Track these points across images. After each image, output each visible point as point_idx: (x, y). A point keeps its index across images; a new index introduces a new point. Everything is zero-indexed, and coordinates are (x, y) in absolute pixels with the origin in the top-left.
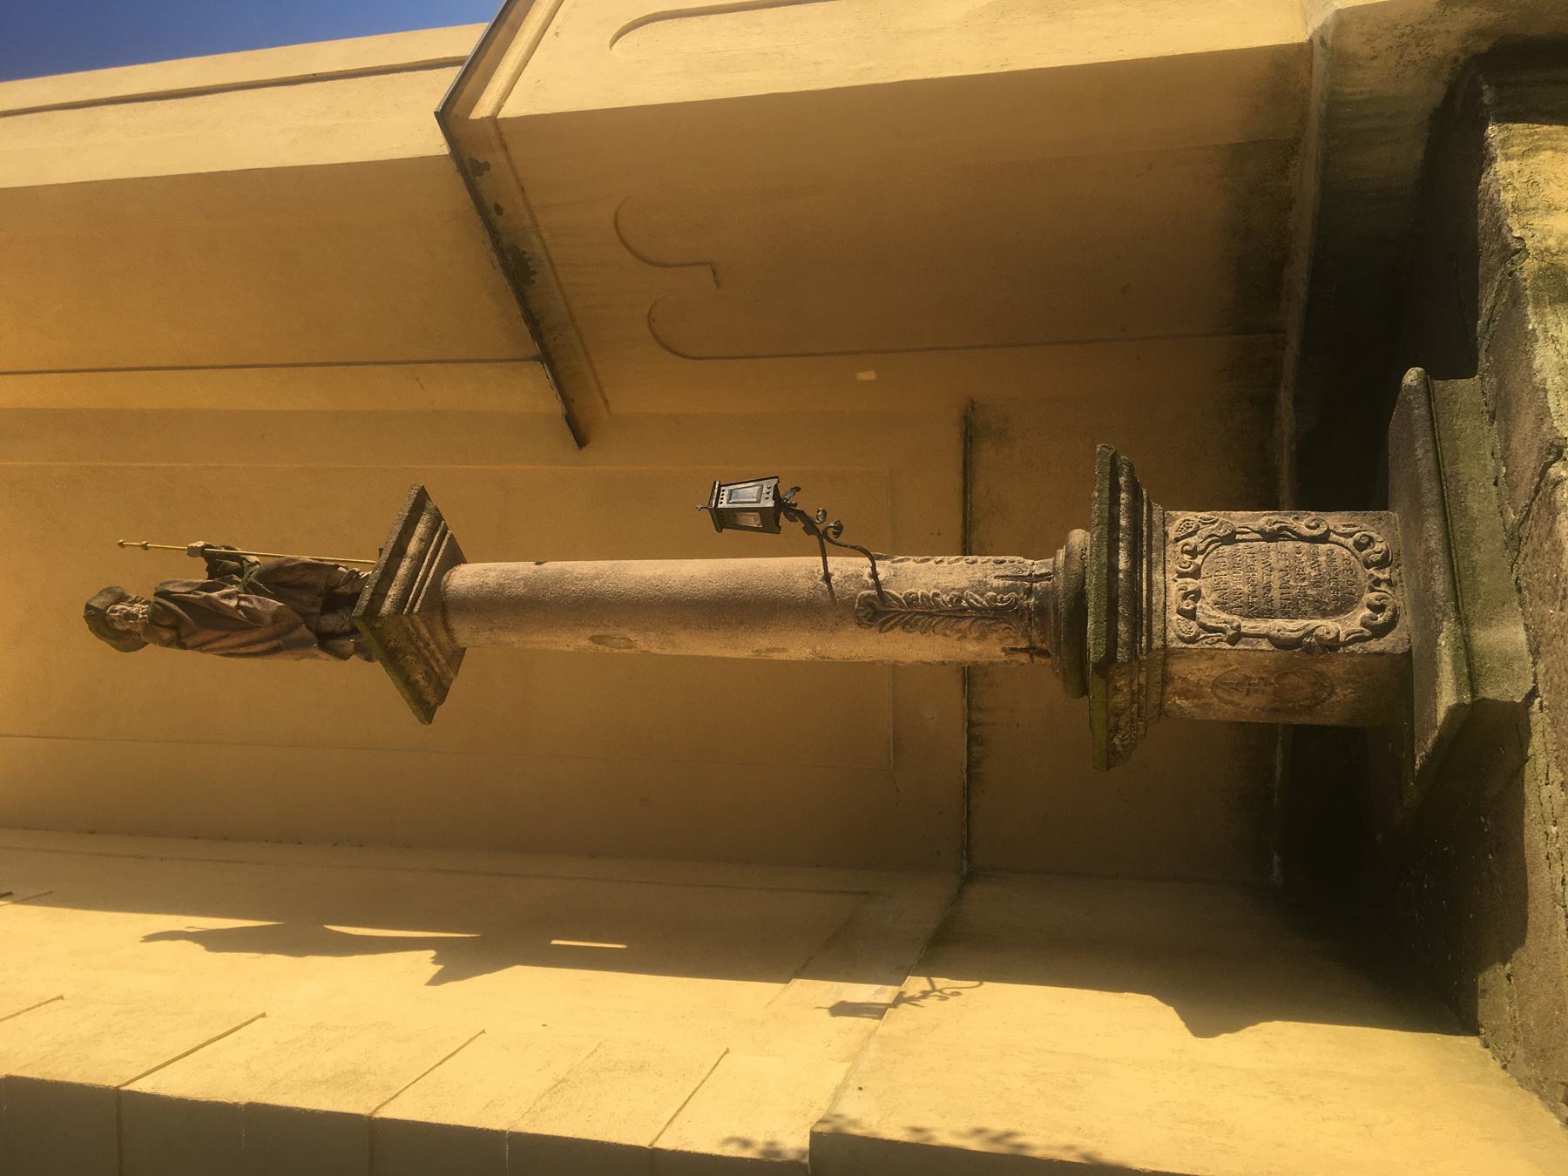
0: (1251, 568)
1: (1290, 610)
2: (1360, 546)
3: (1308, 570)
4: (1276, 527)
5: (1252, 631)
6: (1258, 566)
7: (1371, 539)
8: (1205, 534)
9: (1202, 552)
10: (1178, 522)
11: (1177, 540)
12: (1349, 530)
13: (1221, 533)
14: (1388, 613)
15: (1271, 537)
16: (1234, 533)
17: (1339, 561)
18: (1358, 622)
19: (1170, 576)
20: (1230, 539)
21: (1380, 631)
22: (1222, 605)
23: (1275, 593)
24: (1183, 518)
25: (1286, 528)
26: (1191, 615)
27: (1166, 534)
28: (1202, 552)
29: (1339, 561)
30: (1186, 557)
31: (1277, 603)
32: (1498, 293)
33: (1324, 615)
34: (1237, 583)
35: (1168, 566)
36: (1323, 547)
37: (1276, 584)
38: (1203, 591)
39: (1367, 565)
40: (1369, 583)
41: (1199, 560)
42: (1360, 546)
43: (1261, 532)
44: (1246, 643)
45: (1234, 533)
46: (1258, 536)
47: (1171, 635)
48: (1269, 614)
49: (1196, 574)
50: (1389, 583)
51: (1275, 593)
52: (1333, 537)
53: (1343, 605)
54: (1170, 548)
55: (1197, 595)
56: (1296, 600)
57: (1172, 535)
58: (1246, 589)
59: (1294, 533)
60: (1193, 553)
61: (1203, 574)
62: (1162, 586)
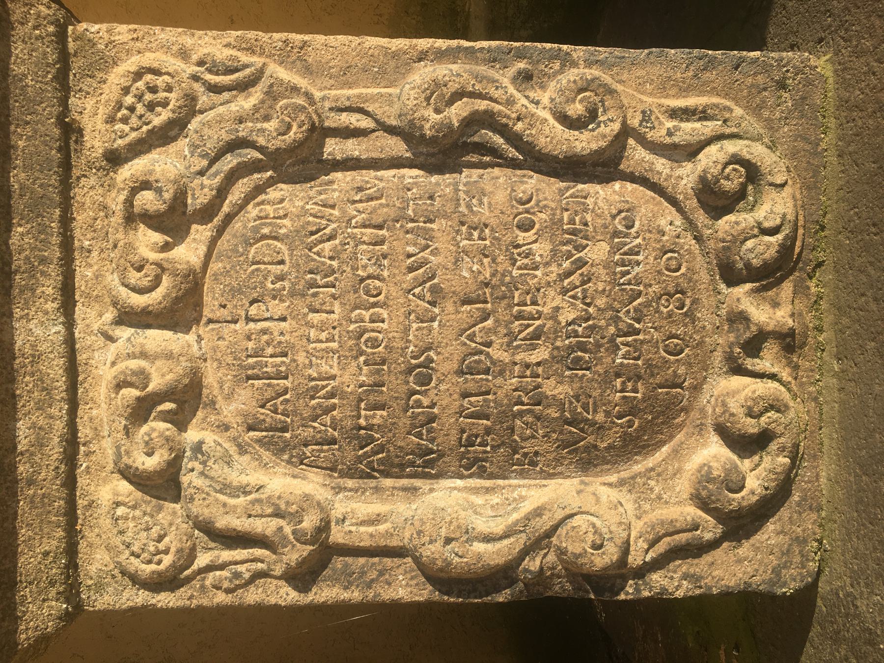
0: (364, 291)
1: (490, 449)
2: (716, 199)
3: (552, 300)
4: (457, 112)
5: (364, 535)
6: (394, 284)
7: (753, 172)
8: (217, 136)
9: (206, 214)
10: (116, 77)
11: (114, 159)
12: (691, 130)
13: (269, 133)
14: (774, 461)
15: (441, 153)
16: (319, 133)
17: (646, 264)
18: (684, 486)
19: (91, 318)
20: (302, 161)
21: (741, 524)
22: (275, 437)
23: (444, 395)
24: (144, 55)
25: (487, 120)
26: (163, 485)
27: (70, 131)
28: (206, 214)
29: (646, 264)
30: (147, 240)
31: (448, 428)
32: (686, 114)
33: (589, 461)
34: (323, 354)
35: (84, 273)
36: (604, 196)
37: (446, 361)
38: (211, 377)
39: (731, 275)
40: (723, 340)
41: (189, 252)
42: (716, 199)
43: (407, 133)
44: (347, 579)
45: (319, 133)
46: (397, 147)
47: (96, 561)
48: (424, 464)
49: (182, 312)
50: (789, 342)
51: (444, 395)
52: (637, 156)
53: (650, 421)
54: (88, 192)
55: (187, 399)
56: (506, 416)
57: (96, 139)
58: (351, 377)
59: (514, 139)
60: (173, 221)
61: (210, 306)
62: (55, 369)
